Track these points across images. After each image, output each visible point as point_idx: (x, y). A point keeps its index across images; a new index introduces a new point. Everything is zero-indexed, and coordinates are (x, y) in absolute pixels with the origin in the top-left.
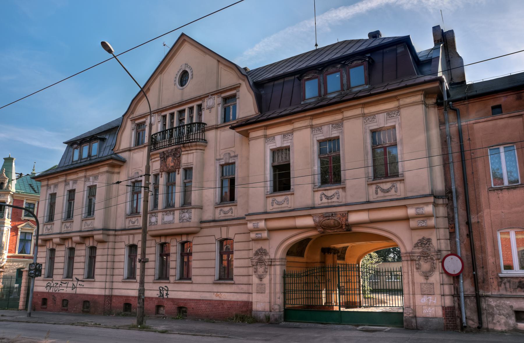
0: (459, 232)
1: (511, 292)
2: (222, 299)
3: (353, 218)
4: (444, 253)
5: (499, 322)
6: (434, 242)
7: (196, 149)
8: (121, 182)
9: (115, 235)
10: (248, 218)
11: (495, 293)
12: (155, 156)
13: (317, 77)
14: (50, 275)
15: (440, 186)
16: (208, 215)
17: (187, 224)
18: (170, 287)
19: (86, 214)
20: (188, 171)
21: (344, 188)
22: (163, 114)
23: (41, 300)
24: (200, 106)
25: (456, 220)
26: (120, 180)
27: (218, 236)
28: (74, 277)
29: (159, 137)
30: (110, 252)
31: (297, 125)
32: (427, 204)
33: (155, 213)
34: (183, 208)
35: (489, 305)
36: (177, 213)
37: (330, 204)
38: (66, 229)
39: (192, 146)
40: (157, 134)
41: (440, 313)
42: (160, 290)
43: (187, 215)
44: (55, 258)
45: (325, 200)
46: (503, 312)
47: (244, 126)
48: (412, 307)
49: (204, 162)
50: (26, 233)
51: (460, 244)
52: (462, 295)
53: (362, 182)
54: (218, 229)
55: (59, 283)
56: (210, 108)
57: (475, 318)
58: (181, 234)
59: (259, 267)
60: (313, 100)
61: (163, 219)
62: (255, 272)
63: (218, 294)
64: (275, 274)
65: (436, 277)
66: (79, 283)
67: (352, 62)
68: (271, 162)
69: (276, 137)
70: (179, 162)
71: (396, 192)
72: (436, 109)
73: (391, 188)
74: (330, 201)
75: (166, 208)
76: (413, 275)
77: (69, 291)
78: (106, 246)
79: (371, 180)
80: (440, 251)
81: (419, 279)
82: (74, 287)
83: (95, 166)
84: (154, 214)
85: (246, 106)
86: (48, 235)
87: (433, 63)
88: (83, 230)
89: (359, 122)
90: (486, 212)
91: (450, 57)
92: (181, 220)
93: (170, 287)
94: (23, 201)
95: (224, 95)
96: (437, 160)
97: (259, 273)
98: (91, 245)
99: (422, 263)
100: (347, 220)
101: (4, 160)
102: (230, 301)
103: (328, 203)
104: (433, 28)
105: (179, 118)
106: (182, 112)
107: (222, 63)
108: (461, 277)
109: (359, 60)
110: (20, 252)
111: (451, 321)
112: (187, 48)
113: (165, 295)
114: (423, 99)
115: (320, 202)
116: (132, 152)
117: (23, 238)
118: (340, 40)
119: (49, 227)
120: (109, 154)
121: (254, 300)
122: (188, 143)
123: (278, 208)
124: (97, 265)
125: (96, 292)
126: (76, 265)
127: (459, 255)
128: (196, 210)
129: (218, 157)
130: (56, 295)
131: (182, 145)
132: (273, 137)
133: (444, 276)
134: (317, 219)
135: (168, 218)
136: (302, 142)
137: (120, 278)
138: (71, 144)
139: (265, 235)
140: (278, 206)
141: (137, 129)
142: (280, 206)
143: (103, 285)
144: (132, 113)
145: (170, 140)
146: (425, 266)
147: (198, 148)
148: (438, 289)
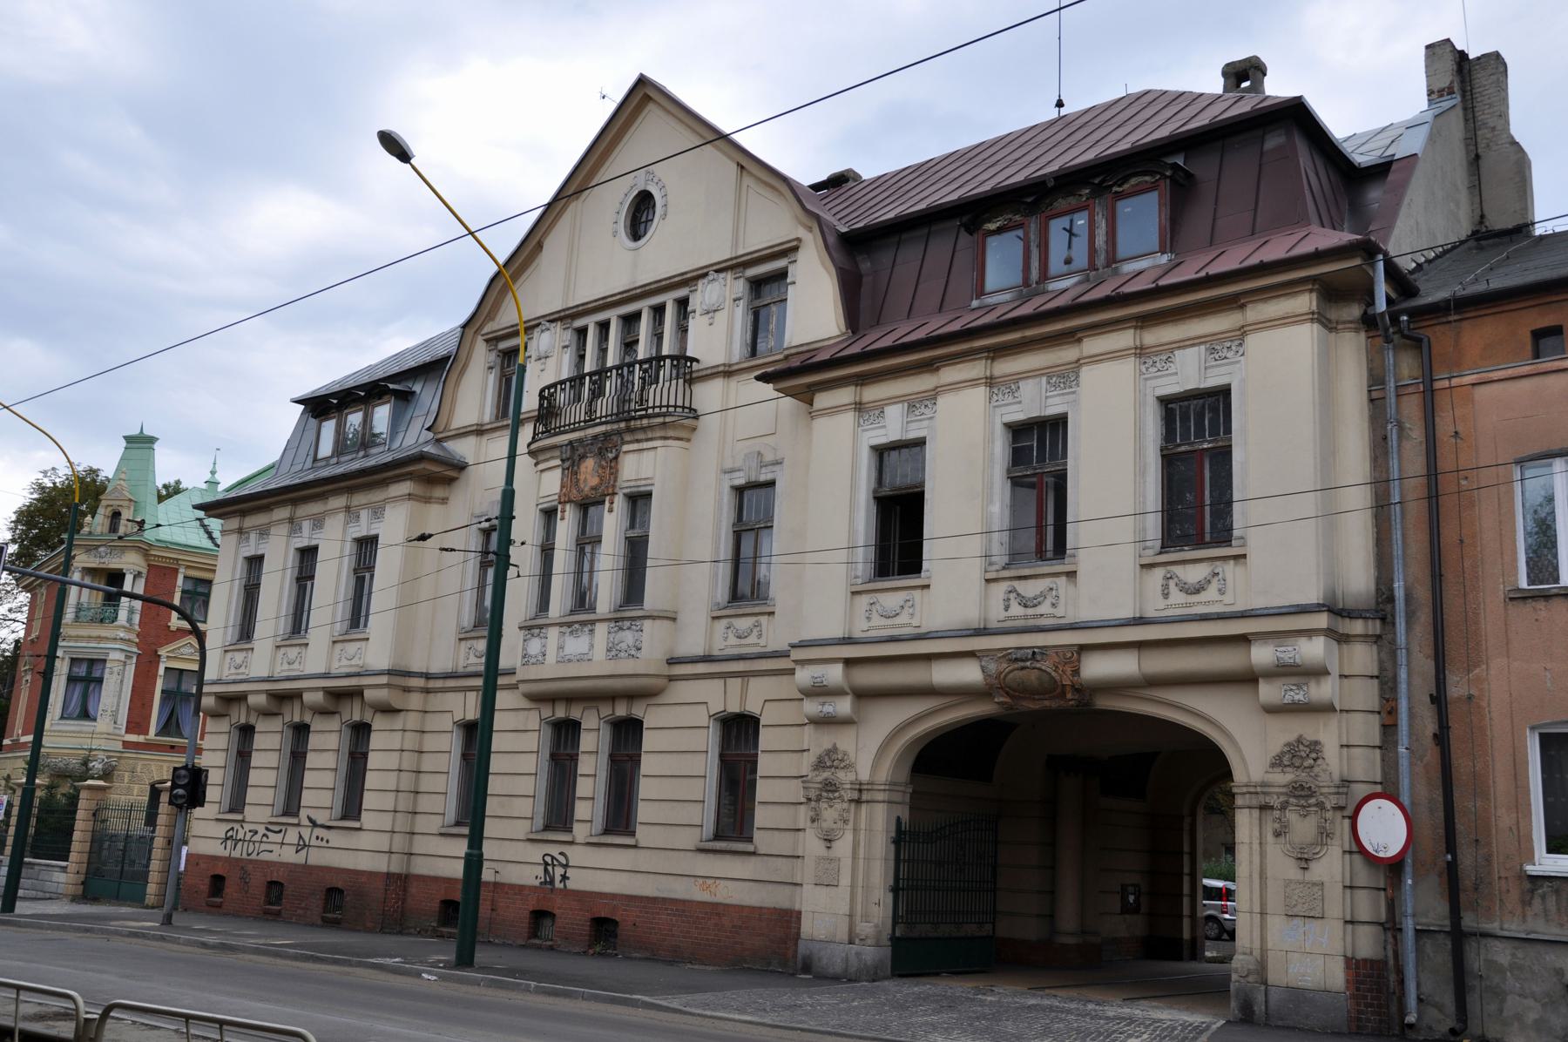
0: (1411, 726)
1: (1562, 925)
2: (719, 899)
3: (1097, 668)
4: (1361, 790)
5: (1519, 1017)
6: (1331, 751)
7: (665, 438)
8: (430, 536)
9: (427, 691)
10: (797, 654)
11: (1514, 927)
12: (548, 455)
13: (1020, 226)
14: (237, 803)
15: (1358, 579)
16: (692, 644)
17: (626, 667)
18: (576, 855)
19: (347, 624)
20: (639, 500)
21: (1071, 575)
22: (579, 323)
23: (207, 881)
24: (683, 303)
25: (1403, 687)
26: (427, 532)
27: (716, 707)
28: (303, 813)
29: (561, 398)
30: (410, 741)
31: (949, 374)
32: (1309, 633)
33: (541, 627)
34: (619, 615)
35: (1491, 964)
36: (601, 630)
37: (1031, 623)
38: (286, 667)
39: (650, 427)
40: (554, 385)
41: (1336, 977)
42: (546, 864)
43: (628, 637)
44: (254, 754)
45: (1016, 610)
46: (1534, 988)
47: (801, 375)
48: (1257, 953)
49: (682, 481)
50: (182, 671)
51: (1411, 764)
52: (1409, 925)
53: (974, 571)
54: (718, 684)
55: (262, 830)
56: (711, 312)
57: (1448, 1000)
58: (612, 697)
59: (823, 805)
60: (1007, 297)
61: (561, 648)
62: (813, 821)
63: (709, 882)
64: (870, 830)
65: (1331, 866)
66: (318, 832)
67: (1125, 179)
68: (873, 485)
69: (887, 409)
70: (615, 473)
71: (1221, 592)
72: (1363, 335)
73: (1043, 595)
74: (1030, 611)
75: (572, 612)
76: (1263, 855)
77: (289, 855)
78: (398, 722)
79: (1151, 552)
80: (1346, 782)
81: (1282, 867)
82: (302, 846)
83: (376, 477)
84: (536, 631)
85: (814, 311)
86: (234, 682)
87: (1391, 177)
88: (334, 671)
89: (1128, 367)
90: (1497, 664)
91: (1482, 145)
92: (613, 651)
93: (576, 855)
94: (176, 571)
95: (752, 272)
96: (1357, 499)
97: (825, 825)
98: (356, 717)
99: (1292, 816)
100: (1076, 672)
101: (124, 443)
102: (740, 908)
103: (1026, 617)
104: (1428, 47)
105: (623, 338)
106: (631, 320)
107: (750, 173)
108: (1408, 869)
109: (1145, 173)
110: (164, 730)
111: (1371, 1005)
112: (652, 123)
113: (558, 878)
114: (1314, 308)
115: (1003, 615)
116: (486, 437)
117: (172, 686)
118: (1136, 88)
119: (239, 657)
120: (421, 440)
121: (805, 908)
122: (641, 417)
123: (885, 627)
124: (371, 780)
125: (365, 863)
126: (309, 779)
127: (1405, 800)
128: (658, 622)
129: (728, 465)
130: (250, 868)
131: (623, 425)
132: (879, 407)
133: (1357, 858)
134: (993, 667)
135: (576, 645)
136: (961, 430)
137: (434, 824)
138: (319, 406)
139: (844, 706)
140: (884, 622)
141: (502, 368)
142: (889, 622)
143: (383, 842)
144: (491, 317)
145: (590, 411)
146: (1303, 827)
147: (671, 433)
148: (1335, 905)
